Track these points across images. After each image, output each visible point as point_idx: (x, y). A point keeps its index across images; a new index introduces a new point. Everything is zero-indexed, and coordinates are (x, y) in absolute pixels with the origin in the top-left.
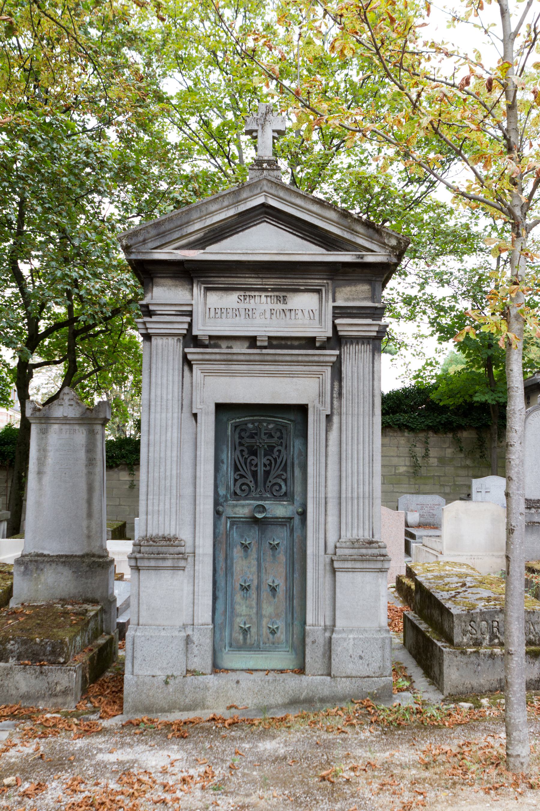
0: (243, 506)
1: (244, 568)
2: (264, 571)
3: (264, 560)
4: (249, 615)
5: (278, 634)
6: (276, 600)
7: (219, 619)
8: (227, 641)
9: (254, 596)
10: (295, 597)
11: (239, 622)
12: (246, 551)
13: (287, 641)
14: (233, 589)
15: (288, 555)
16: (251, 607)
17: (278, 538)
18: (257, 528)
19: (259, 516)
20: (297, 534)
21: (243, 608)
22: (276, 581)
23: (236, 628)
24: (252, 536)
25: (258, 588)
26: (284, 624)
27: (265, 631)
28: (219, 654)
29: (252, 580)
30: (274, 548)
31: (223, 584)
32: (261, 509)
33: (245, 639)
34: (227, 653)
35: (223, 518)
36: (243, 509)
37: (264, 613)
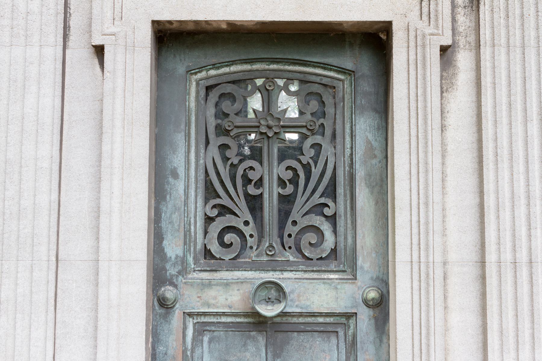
0: (227, 285)
19: (268, 311)
32: (273, 293)
35: (177, 317)
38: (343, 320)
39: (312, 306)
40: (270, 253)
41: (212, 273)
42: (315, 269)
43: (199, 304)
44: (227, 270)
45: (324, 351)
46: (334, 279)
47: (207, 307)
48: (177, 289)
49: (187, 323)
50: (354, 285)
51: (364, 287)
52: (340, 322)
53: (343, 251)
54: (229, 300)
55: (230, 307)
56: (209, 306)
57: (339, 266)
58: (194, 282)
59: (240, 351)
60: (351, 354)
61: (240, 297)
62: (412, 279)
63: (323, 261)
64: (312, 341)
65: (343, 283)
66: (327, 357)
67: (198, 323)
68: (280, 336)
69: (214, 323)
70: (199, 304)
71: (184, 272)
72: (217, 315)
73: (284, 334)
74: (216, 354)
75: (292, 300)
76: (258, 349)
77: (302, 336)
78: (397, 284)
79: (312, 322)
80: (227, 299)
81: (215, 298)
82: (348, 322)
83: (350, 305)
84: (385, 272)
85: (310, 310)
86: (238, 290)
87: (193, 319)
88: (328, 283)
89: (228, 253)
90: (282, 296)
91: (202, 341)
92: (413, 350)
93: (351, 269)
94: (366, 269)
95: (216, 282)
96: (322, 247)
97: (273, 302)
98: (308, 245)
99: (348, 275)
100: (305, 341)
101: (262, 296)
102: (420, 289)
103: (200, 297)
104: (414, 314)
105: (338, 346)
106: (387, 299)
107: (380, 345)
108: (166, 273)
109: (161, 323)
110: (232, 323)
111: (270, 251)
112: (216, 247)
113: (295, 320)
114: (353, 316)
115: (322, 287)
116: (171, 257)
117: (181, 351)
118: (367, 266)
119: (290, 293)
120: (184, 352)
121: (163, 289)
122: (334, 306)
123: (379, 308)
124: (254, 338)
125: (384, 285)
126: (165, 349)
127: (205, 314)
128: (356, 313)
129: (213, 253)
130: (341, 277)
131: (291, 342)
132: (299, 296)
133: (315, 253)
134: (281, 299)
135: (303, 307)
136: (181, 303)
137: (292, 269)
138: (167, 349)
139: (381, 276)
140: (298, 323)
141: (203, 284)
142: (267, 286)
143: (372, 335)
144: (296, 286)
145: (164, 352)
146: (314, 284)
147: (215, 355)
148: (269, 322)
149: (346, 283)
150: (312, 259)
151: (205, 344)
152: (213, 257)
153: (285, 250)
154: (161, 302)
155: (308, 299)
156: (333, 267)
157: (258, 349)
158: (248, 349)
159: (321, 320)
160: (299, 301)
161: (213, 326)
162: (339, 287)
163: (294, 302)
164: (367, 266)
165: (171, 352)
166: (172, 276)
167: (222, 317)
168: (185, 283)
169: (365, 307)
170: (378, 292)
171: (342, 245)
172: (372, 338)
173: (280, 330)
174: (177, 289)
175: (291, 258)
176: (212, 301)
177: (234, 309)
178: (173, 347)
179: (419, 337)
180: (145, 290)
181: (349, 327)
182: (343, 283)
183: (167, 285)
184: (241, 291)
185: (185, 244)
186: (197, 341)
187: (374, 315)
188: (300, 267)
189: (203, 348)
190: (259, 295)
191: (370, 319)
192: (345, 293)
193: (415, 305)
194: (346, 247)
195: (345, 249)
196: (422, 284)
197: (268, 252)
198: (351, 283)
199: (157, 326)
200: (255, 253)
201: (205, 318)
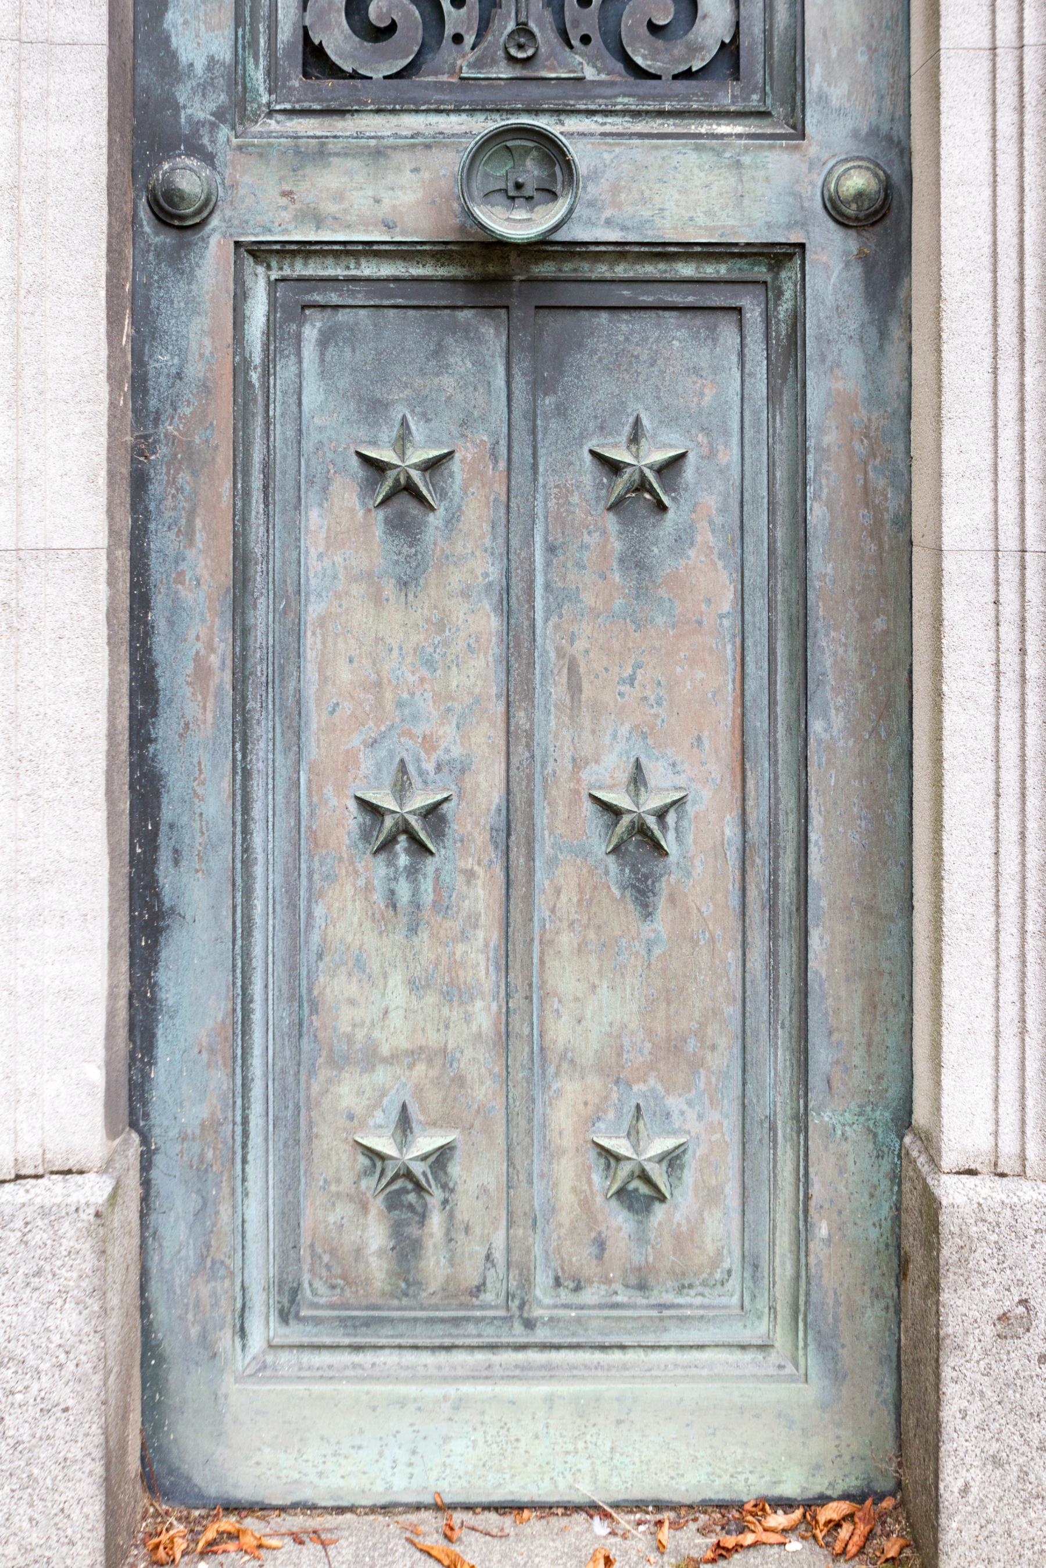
0: (378, 153)
1: (387, 661)
2: (558, 690)
3: (561, 598)
4: (444, 1055)
5: (683, 1203)
6: (662, 924)
7: (187, 1088)
8: (259, 1270)
9: (481, 897)
10: (819, 902)
11: (356, 1109)
12: (402, 528)
13: (752, 1264)
14: (299, 840)
15: (757, 562)
16: (455, 993)
17: (670, 418)
18: (492, 336)
19: (516, 225)
20: (835, 377)
21: (391, 996)
22: (657, 773)
23: (334, 1160)
24: (457, 393)
25: (513, 831)
26: (725, 1120)
27: (569, 1181)
28: (185, 1383)
29: (461, 769)
30: (642, 495)
31: (214, 802)
32: (531, 171)
33: (406, 1250)
34: (262, 1370)
35: (214, 253)
36: (390, 179)
37: (561, 1032)
38: (760, 272)
39: (657, 220)
40: (521, 55)
41: (327, 121)
42: (667, 106)
43: (286, 215)
44: (378, 111)
45: (696, 371)
46: (730, 135)
47: (313, 227)
48: (215, 168)
49: (249, 283)
50: (797, 156)
51: (833, 153)
52: (750, 276)
53: (760, 49)
54: (386, 202)
55: (389, 226)
56: (319, 221)
57: (747, 99)
58: (270, 145)
59: (422, 372)
60: (785, 380)
61: (420, 194)
62: (994, 103)
63: (694, 83)
64: (657, 340)
65: (761, 146)
66: (706, 391)
67: (283, 280)
68: (556, 324)
69: (335, 279)
70: (286, 215)
71: (238, 110)
72: (348, 253)
73: (567, 319)
74: (344, 382)
75: (591, 204)
76: (482, 365)
77: (625, 325)
78: (944, 121)
79: (658, 276)
80: (377, 201)
81: (339, 196)
82: (776, 278)
83: (782, 220)
84: (899, 112)
85: (650, 236)
86: (416, 170)
87: (269, 267)
88: (713, 149)
89: (384, 57)
90: (559, 178)
91: (299, 338)
92: (996, 335)
93: (787, 111)
94: (835, 103)
95: (341, 143)
96: (691, 36)
97: (531, 198)
98: (644, 30)
99: (775, 125)
100: (636, 338)
101: (496, 178)
102: (1021, 134)
103: (291, 192)
104: (999, 218)
105: (742, 355)
106: (905, 198)
107: (881, 347)
108: (177, 115)
109: (163, 278)
110: (396, 280)
111: (521, 47)
112: (341, 38)
113: (602, 270)
114: (790, 256)
115: (687, 160)
116: (192, 65)
117: (229, 368)
118: (837, 93)
119: (588, 178)
120: (240, 370)
121: (166, 166)
122: (731, 222)
123: (878, 228)
124: (467, 331)
125: (894, 153)
126: (176, 360)
127: (305, 250)
128: (802, 246)
129: (333, 58)
130: (753, 130)
131: (590, 342)
132: (615, 189)
133: (666, 57)
134: (558, 189)
135: (629, 224)
136: (228, 213)
137: (592, 107)
138: (184, 361)
139: (885, 128)
140: (613, 281)
141: (297, 152)
142: (509, 144)
143: (855, 316)
144: (606, 156)
145: (173, 371)
146: (666, 153)
147: (341, 384)
148: (518, 278)
149: (771, 147)
150: (658, 77)
151: (309, 351)
152: (335, 72)
153: (571, 47)
154: (161, 208)
155: (644, 201)
156: (726, 99)
157: (482, 365)
158: (448, 366)
159: (686, 270)
160: (618, 206)
161: (335, 290)
162: (746, 160)
163: (602, 209)
164: (837, 93)
165: (194, 370)
166: (196, 125)
167: (363, 262)
168: (240, 148)
169: (832, 225)
170: (876, 175)
171: (757, 30)
172: (853, 326)
173: (552, 303)
174: (215, 168)
175: (590, 73)
176: (331, 208)
177: (403, 233)
178: (201, 355)
179: (1016, 293)
180: (104, 141)
181: (779, 294)
182: (761, 146)
183: (179, 156)
184: (426, 175)
185: (239, 21)
186: (282, 339)
187: (860, 252)
188: (620, 100)
189: (300, 362)
190: (486, 175)
191: (847, 264)
192: (767, 179)
193: (1001, 189)
194: (771, 35)
195: (768, 42)
196: (1028, 116)
197: (513, 52)
198: (787, 147)
199: (148, 286)
200: (471, 57)
201: (305, 265)
